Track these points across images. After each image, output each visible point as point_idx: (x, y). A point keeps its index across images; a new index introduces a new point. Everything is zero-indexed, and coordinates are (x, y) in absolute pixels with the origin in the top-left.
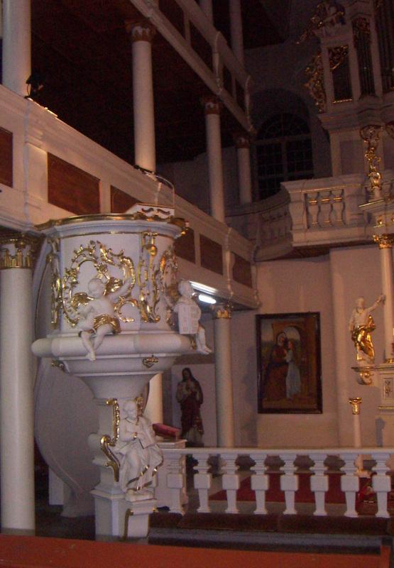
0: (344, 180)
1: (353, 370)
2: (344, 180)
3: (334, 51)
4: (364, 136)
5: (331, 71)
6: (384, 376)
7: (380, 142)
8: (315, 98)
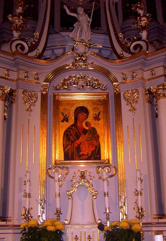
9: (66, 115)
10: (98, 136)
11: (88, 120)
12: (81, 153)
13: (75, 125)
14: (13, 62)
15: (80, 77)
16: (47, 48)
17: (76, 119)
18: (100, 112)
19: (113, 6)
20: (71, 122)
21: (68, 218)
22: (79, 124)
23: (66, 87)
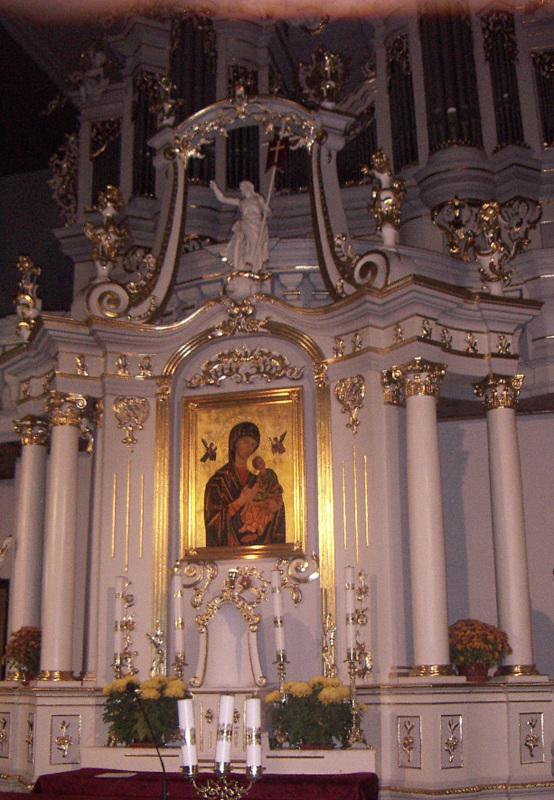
3: (99, 125)
4: (128, 267)
5: (91, 159)
8: (60, 204)
9: (212, 444)
10: (280, 490)
11: (259, 452)
12: (243, 530)
13: (229, 467)
14: (91, 338)
15: (243, 354)
16: (176, 287)
17: (232, 454)
18: (285, 434)
19: (329, 162)
20: (222, 458)
21: (199, 674)
22: (238, 463)
23: (212, 382)
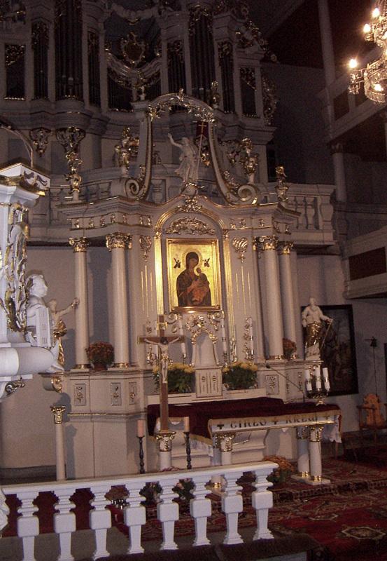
0: (321, 190)
1: (40, 375)
2: (321, 190)
5: (6, 67)
6: (73, 382)
7: (49, 145)
12: (194, 299)
17: (187, 266)
20: (183, 267)
